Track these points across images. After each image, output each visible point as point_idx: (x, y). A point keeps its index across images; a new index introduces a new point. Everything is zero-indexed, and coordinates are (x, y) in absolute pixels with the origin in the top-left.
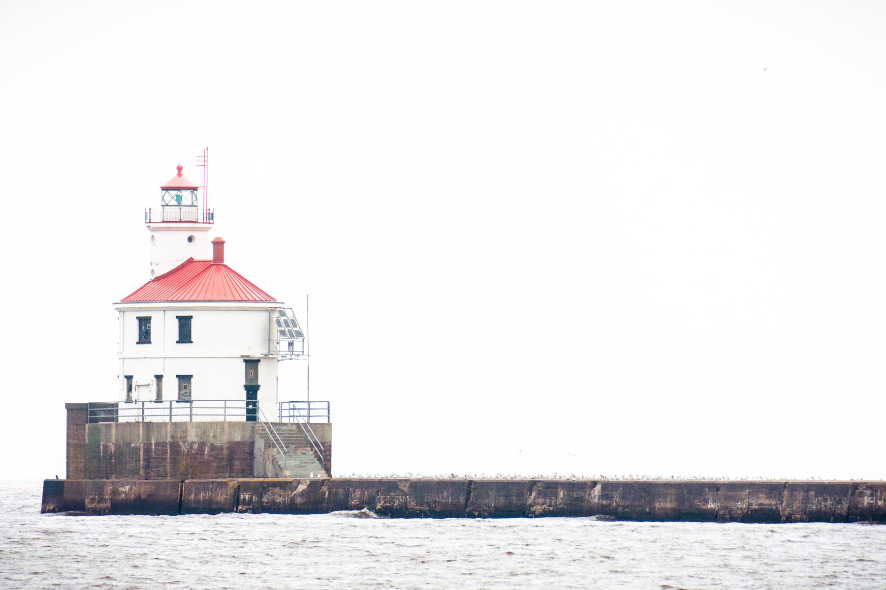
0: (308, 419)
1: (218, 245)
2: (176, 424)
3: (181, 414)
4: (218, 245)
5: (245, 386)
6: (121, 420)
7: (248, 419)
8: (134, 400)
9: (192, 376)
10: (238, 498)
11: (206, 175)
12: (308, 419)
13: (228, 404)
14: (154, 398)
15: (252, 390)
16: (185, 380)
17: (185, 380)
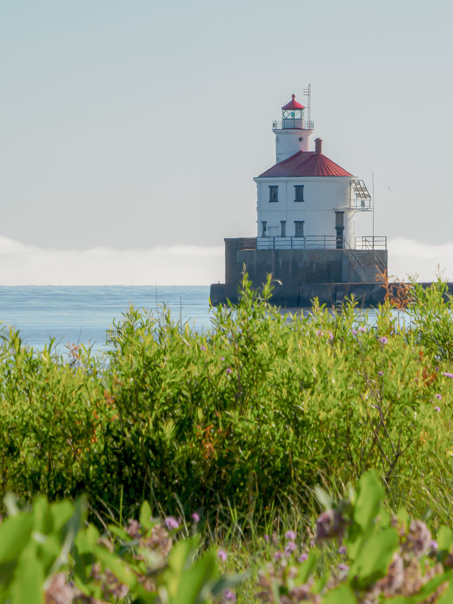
0: (373, 248)
1: (318, 142)
2: (295, 250)
3: (298, 244)
4: (318, 142)
6: (259, 248)
7: (338, 247)
8: (267, 235)
9: (303, 222)
10: (336, 295)
11: (309, 100)
12: (373, 248)
13: (327, 238)
14: (280, 234)
15: (340, 230)
16: (299, 224)
17: (299, 224)
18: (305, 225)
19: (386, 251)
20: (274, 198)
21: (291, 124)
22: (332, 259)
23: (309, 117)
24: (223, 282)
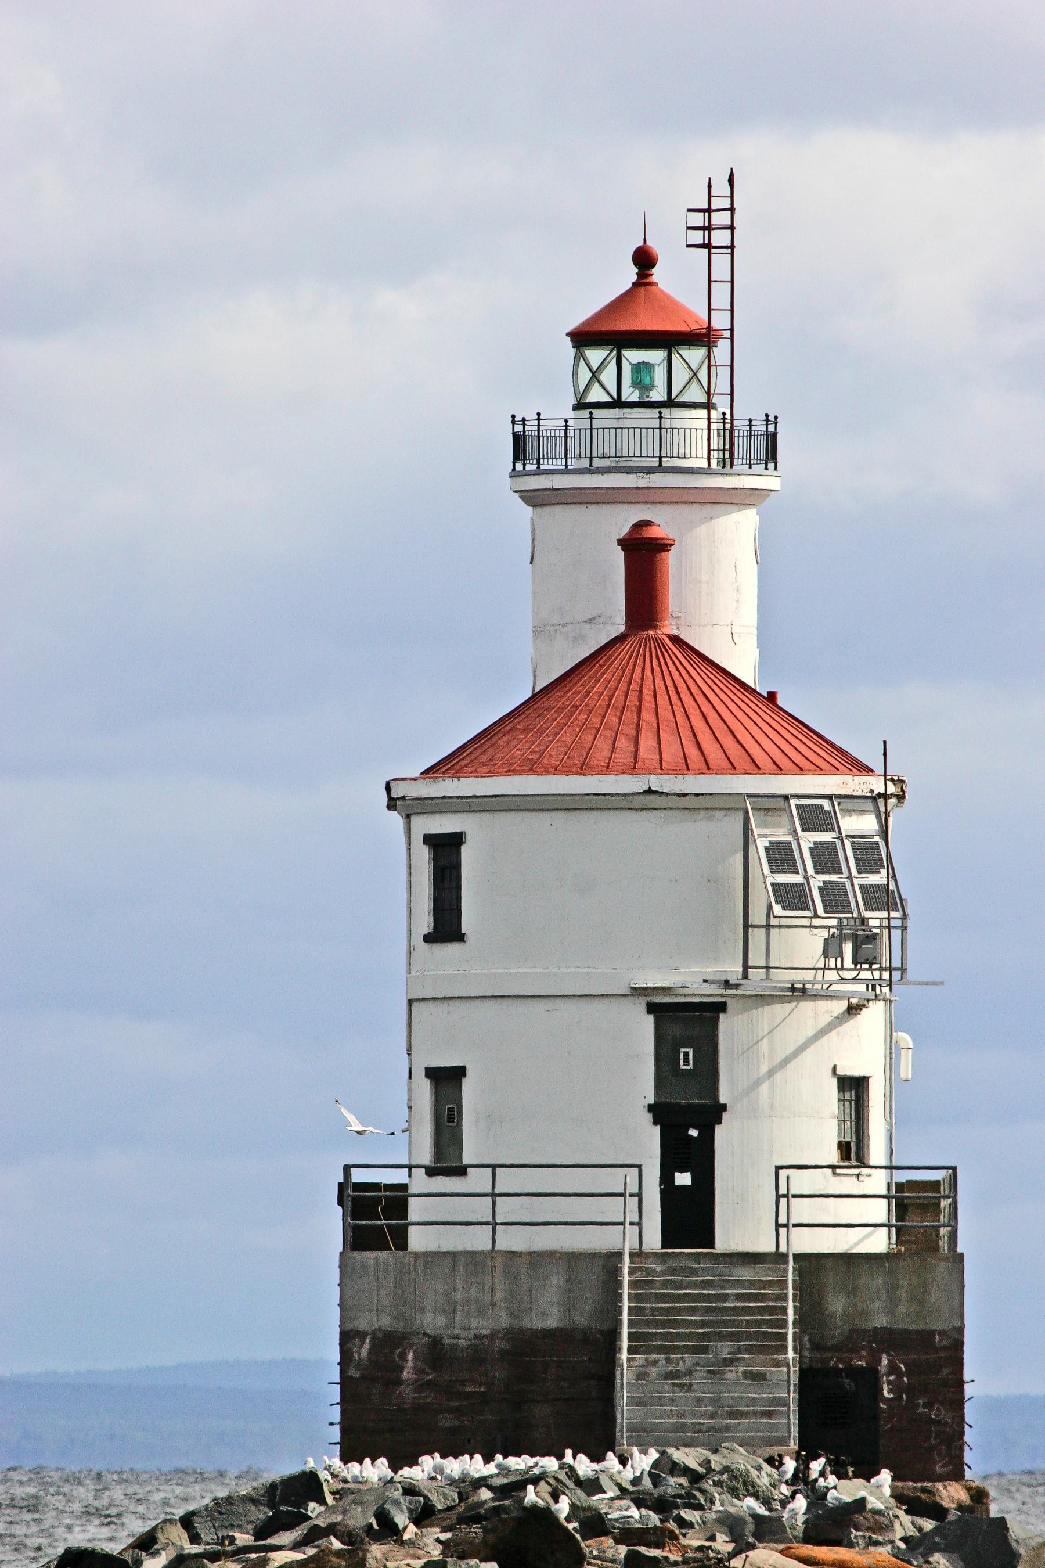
5: (651, 1108)
13: (507, 1181)
15: (688, 1122)
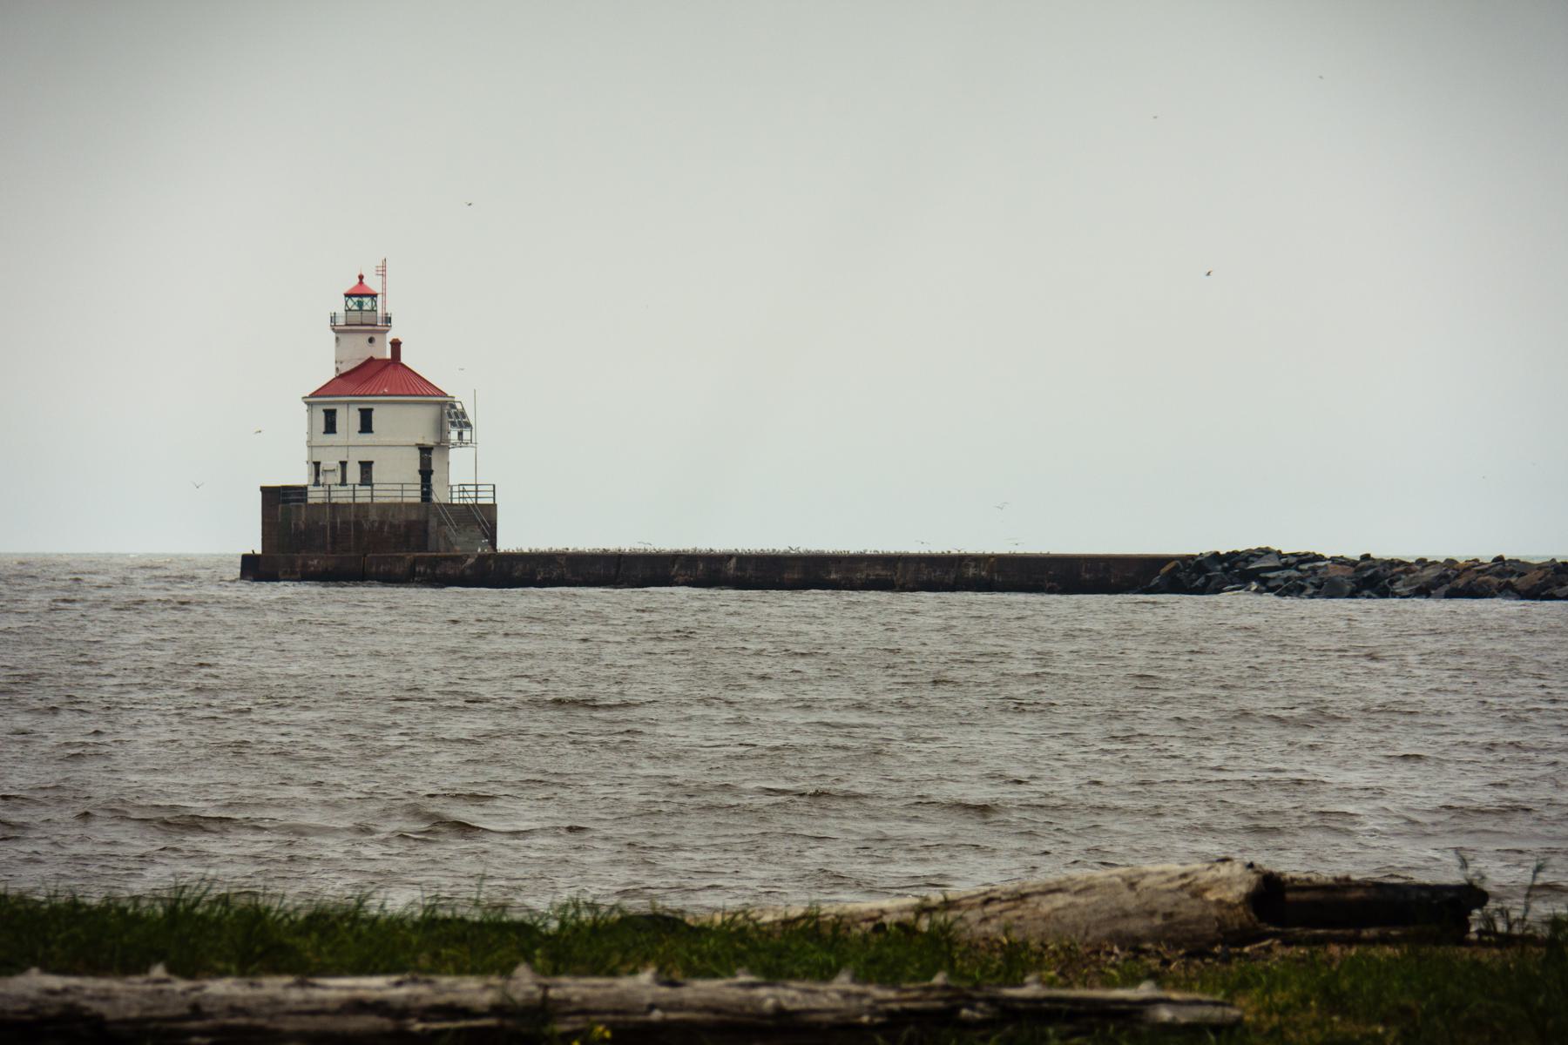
3: (363, 496)
4: (396, 345)
6: (310, 501)
11: (384, 283)
15: (426, 473)
16: (366, 466)
17: (366, 466)
18: (374, 467)
19: (494, 506)
20: (330, 427)
21: (362, 311)
22: (414, 517)
23: (384, 308)
24: (259, 551)
